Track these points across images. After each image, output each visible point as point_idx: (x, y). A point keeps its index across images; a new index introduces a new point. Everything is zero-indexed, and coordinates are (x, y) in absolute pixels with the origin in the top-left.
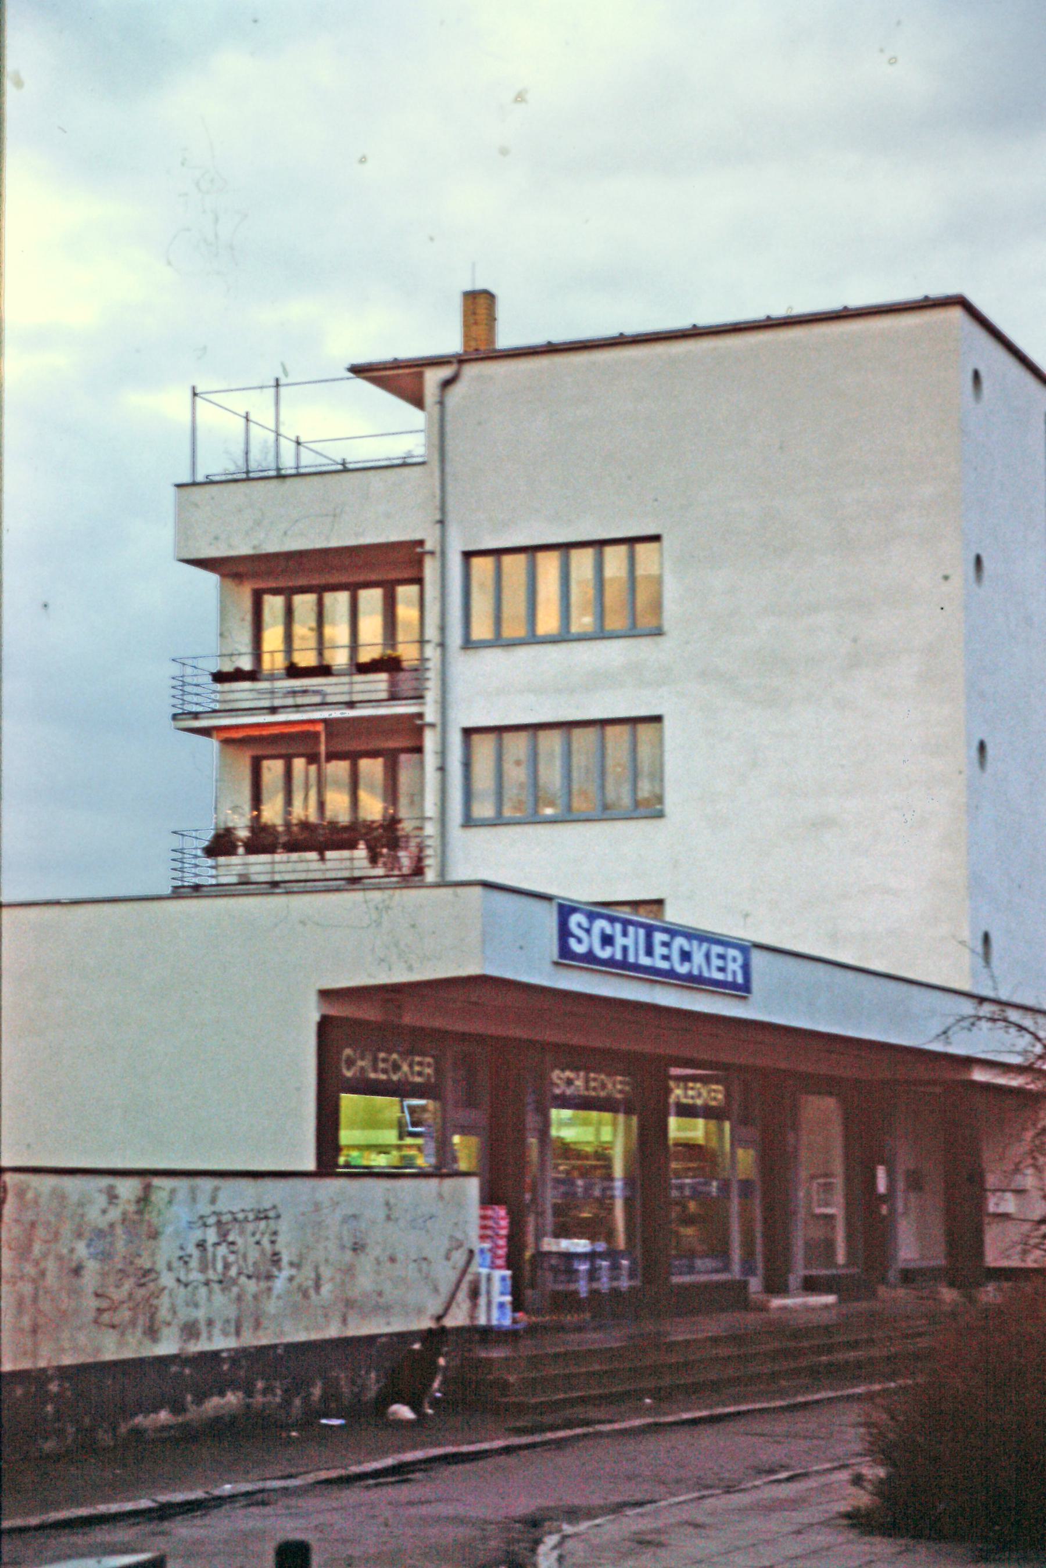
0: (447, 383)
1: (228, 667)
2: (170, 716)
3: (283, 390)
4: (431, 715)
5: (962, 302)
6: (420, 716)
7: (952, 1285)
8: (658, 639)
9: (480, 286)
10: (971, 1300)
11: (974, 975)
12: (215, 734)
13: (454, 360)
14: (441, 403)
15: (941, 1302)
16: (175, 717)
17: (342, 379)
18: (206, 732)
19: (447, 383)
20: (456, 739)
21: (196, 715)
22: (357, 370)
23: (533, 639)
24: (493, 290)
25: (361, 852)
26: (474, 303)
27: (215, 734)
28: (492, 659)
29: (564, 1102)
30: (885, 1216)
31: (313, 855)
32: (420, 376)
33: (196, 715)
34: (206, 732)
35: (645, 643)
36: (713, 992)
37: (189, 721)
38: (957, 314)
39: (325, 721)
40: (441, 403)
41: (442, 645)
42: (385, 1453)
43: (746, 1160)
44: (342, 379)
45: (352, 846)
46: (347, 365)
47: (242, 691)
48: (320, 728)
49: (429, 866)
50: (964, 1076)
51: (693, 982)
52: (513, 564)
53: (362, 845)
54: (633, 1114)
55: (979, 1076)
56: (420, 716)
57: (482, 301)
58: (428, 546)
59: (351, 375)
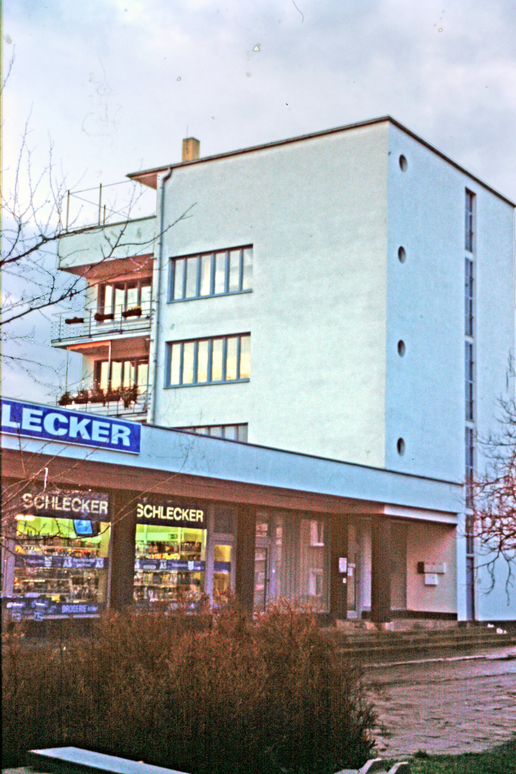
0: (166, 179)
1: (71, 317)
2: (251, 380)
3: (103, 188)
4: (153, 337)
5: (389, 119)
6: (149, 336)
7: (373, 621)
8: (251, 294)
9: (189, 136)
10: (379, 628)
11: (387, 458)
12: (68, 348)
13: (169, 168)
14: (163, 188)
15: (366, 629)
16: (52, 341)
17: (125, 182)
18: (64, 347)
19: (166, 179)
20: (163, 347)
21: (60, 340)
22: (131, 176)
23: (199, 297)
24: (197, 137)
25: (121, 403)
26: (187, 144)
27: (68, 348)
28: (179, 309)
29: (144, 521)
30: (345, 584)
31: (101, 404)
32: (155, 176)
33: (60, 340)
34: (64, 347)
35: (245, 296)
36: (82, 446)
37: (59, 344)
38: (387, 125)
39: (112, 341)
40: (163, 188)
41: (159, 302)
42: (461, 656)
43: (226, 552)
44: (125, 182)
45: (118, 400)
46: (126, 174)
47: (77, 328)
48: (109, 344)
49: (149, 408)
50: (380, 512)
51: (72, 442)
52: (193, 262)
53: (121, 399)
54: (205, 529)
55: (387, 511)
56: (149, 336)
57: (191, 143)
58: (155, 256)
59: (128, 179)
